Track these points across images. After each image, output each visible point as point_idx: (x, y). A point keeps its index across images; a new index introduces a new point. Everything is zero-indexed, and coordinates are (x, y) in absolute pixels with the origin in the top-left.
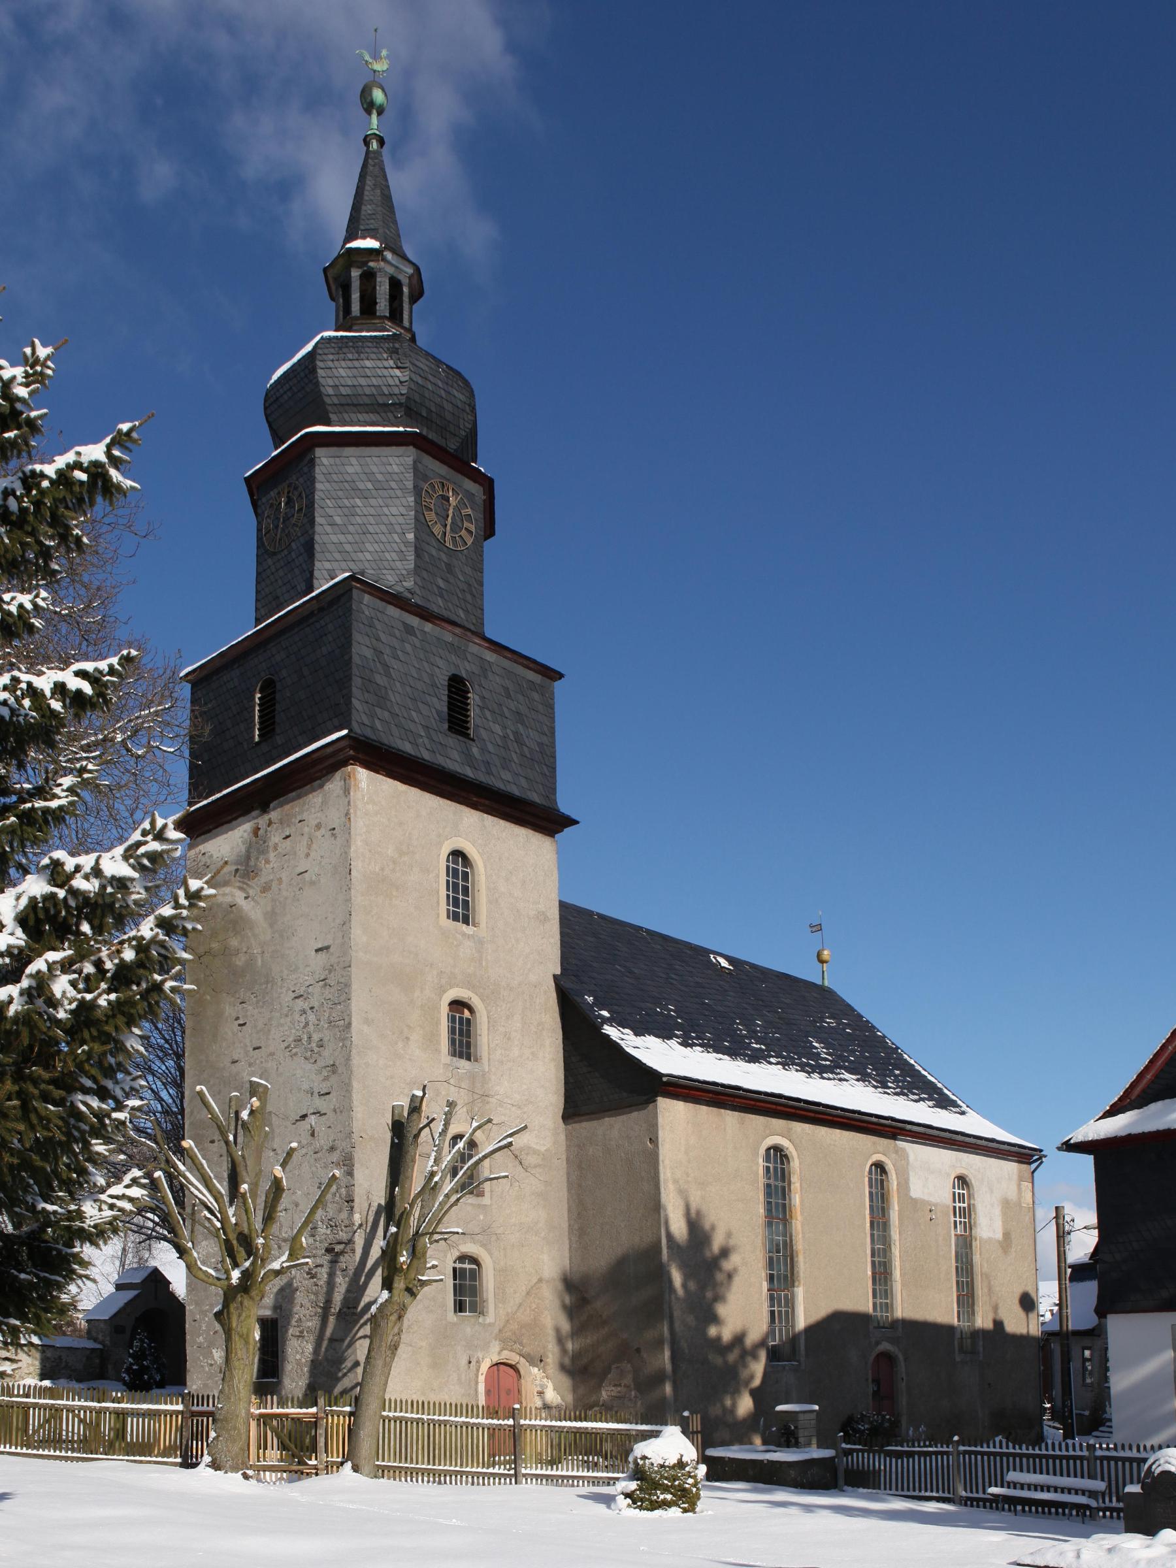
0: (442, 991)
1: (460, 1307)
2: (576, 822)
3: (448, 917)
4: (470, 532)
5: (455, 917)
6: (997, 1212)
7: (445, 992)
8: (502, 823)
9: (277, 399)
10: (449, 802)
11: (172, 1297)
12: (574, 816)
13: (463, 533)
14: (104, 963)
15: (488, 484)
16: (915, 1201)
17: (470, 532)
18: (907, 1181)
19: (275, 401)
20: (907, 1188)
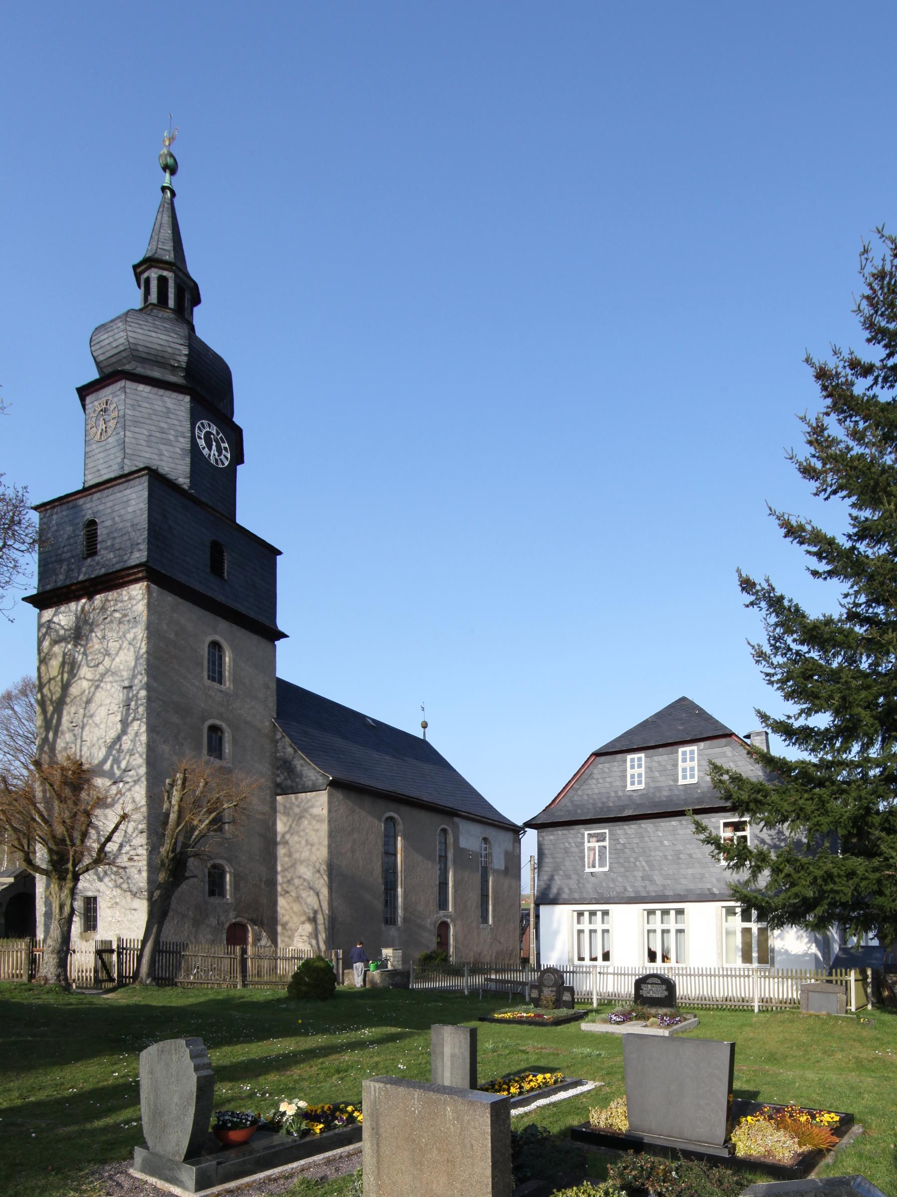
0: (204, 720)
1: (212, 893)
2: (287, 636)
3: (209, 679)
4: (227, 458)
5: (213, 680)
6: (502, 857)
7: (206, 720)
8: (243, 631)
9: (99, 342)
10: (210, 613)
11: (620, 1149)
12: (286, 633)
13: (222, 457)
14: (781, 873)
15: (238, 432)
16: (464, 850)
17: (227, 458)
18: (458, 839)
19: (109, 344)
20: (458, 843)
